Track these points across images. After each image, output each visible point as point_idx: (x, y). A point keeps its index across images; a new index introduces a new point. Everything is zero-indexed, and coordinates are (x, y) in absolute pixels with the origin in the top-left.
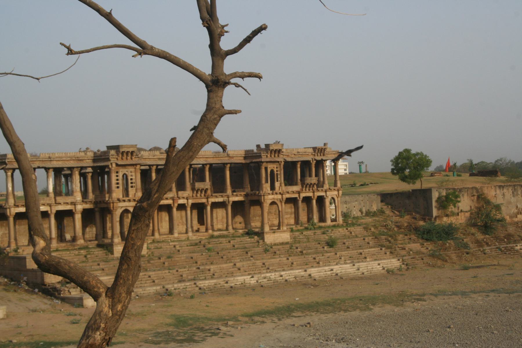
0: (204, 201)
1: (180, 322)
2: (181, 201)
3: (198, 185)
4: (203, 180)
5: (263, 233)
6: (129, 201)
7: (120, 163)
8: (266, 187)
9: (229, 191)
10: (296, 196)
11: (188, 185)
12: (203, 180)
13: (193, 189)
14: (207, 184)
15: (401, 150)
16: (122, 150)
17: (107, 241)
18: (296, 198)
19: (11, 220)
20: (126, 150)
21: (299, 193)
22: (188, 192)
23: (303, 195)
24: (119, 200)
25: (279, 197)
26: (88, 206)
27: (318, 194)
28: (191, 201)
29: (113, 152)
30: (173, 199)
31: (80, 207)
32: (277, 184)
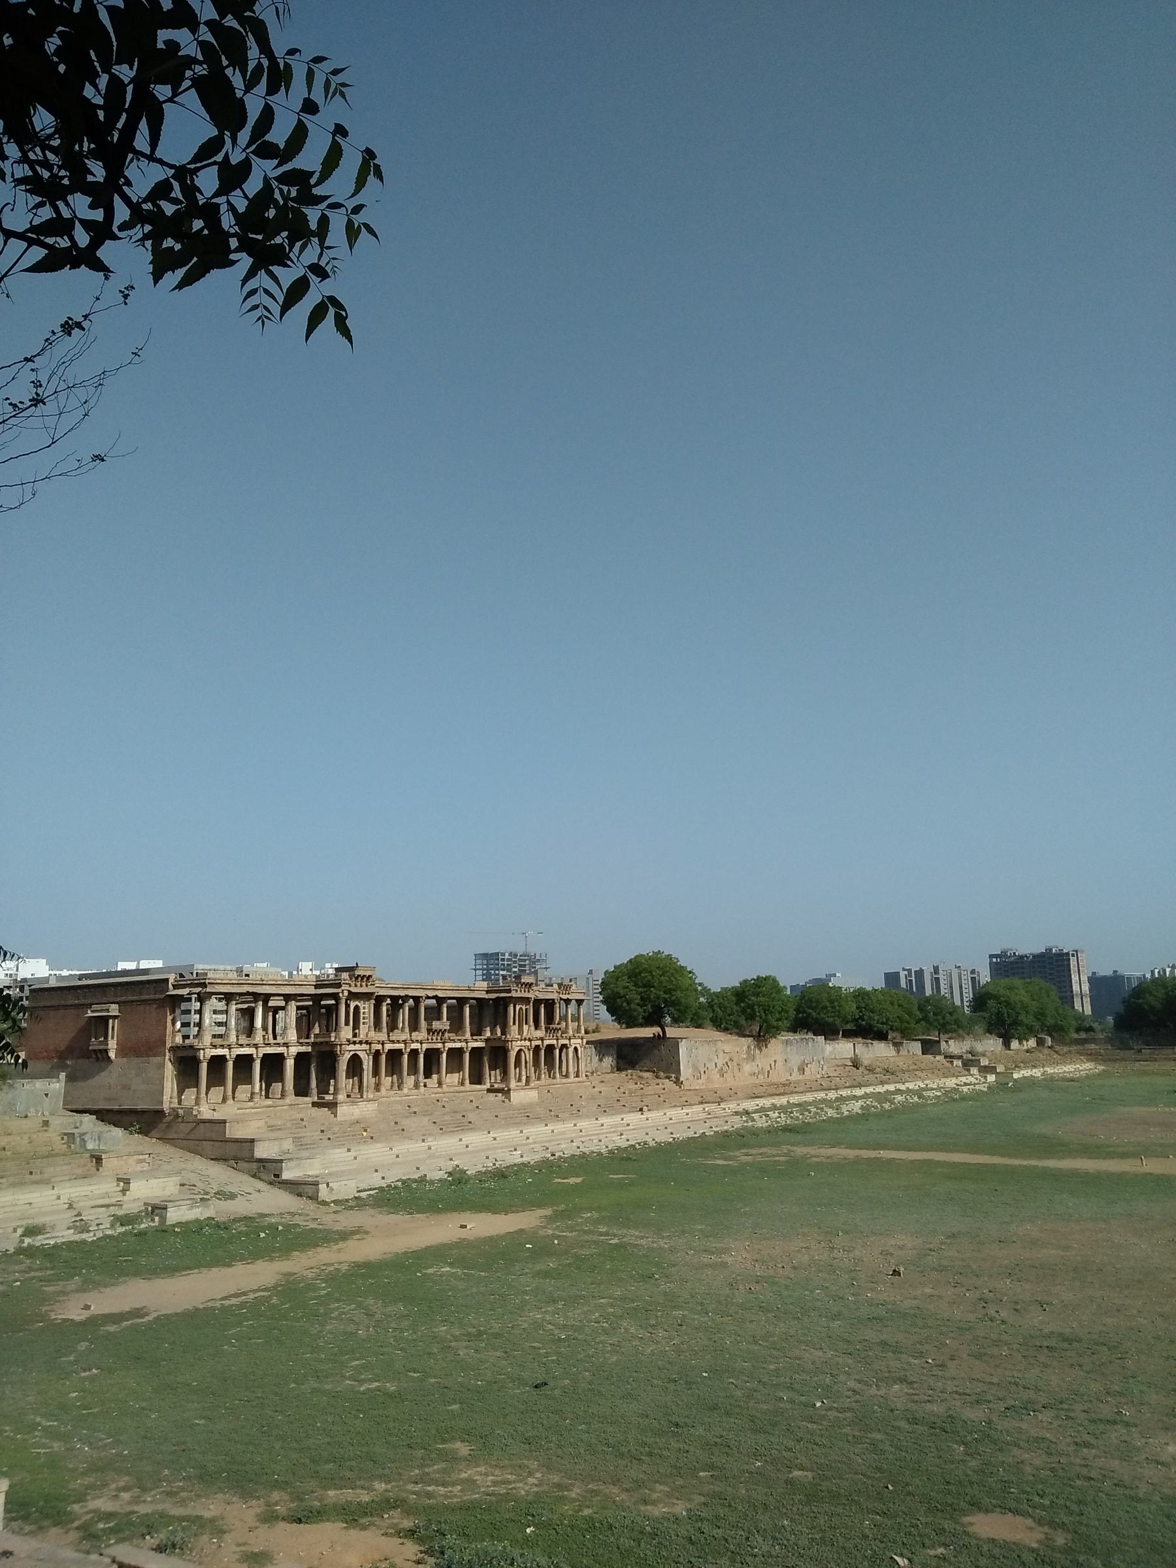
0: (440, 1046)
1: (569, 1218)
2: (415, 1046)
3: (436, 1025)
4: (439, 1018)
5: (509, 1090)
6: (361, 1043)
7: (354, 990)
8: (514, 1029)
9: (468, 1035)
10: (402, 1046)
11: (423, 1024)
12: (439, 1018)
13: (429, 1031)
14: (443, 1024)
15: (751, 975)
16: (357, 973)
17: (329, 1098)
18: (224, 1056)
19: (204, 1067)
20: (362, 973)
21: (542, 1039)
22: (422, 1035)
23: (547, 1042)
24: (348, 1040)
25: (528, 1043)
26: (303, 1049)
27: (562, 1042)
28: (425, 1046)
29: (345, 975)
30: (405, 1042)
31: (294, 1050)
32: (525, 1027)
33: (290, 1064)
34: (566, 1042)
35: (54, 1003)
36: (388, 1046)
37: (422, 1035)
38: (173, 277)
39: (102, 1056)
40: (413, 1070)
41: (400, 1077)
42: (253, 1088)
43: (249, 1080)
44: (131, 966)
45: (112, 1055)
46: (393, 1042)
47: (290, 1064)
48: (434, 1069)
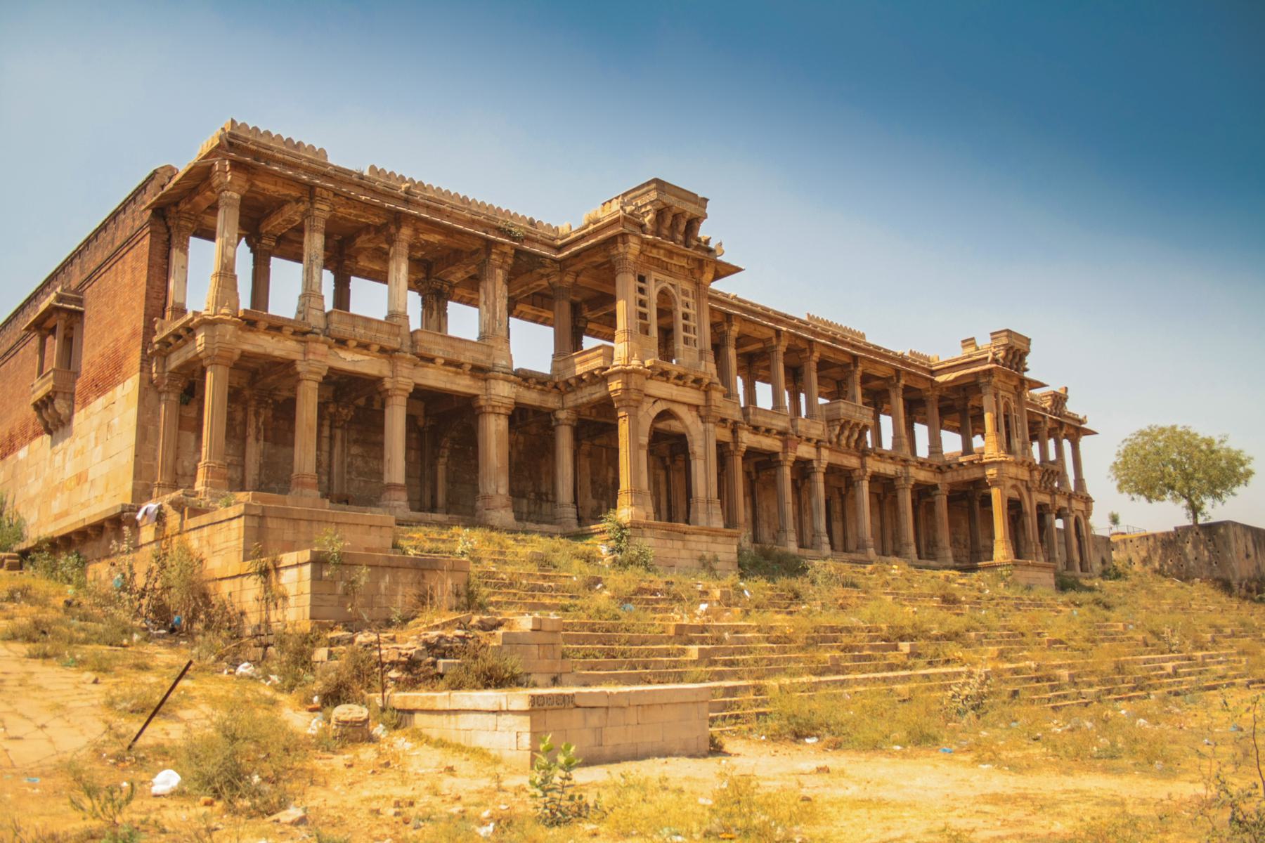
0: (853, 462)
2: (805, 451)
35: (99, 259)
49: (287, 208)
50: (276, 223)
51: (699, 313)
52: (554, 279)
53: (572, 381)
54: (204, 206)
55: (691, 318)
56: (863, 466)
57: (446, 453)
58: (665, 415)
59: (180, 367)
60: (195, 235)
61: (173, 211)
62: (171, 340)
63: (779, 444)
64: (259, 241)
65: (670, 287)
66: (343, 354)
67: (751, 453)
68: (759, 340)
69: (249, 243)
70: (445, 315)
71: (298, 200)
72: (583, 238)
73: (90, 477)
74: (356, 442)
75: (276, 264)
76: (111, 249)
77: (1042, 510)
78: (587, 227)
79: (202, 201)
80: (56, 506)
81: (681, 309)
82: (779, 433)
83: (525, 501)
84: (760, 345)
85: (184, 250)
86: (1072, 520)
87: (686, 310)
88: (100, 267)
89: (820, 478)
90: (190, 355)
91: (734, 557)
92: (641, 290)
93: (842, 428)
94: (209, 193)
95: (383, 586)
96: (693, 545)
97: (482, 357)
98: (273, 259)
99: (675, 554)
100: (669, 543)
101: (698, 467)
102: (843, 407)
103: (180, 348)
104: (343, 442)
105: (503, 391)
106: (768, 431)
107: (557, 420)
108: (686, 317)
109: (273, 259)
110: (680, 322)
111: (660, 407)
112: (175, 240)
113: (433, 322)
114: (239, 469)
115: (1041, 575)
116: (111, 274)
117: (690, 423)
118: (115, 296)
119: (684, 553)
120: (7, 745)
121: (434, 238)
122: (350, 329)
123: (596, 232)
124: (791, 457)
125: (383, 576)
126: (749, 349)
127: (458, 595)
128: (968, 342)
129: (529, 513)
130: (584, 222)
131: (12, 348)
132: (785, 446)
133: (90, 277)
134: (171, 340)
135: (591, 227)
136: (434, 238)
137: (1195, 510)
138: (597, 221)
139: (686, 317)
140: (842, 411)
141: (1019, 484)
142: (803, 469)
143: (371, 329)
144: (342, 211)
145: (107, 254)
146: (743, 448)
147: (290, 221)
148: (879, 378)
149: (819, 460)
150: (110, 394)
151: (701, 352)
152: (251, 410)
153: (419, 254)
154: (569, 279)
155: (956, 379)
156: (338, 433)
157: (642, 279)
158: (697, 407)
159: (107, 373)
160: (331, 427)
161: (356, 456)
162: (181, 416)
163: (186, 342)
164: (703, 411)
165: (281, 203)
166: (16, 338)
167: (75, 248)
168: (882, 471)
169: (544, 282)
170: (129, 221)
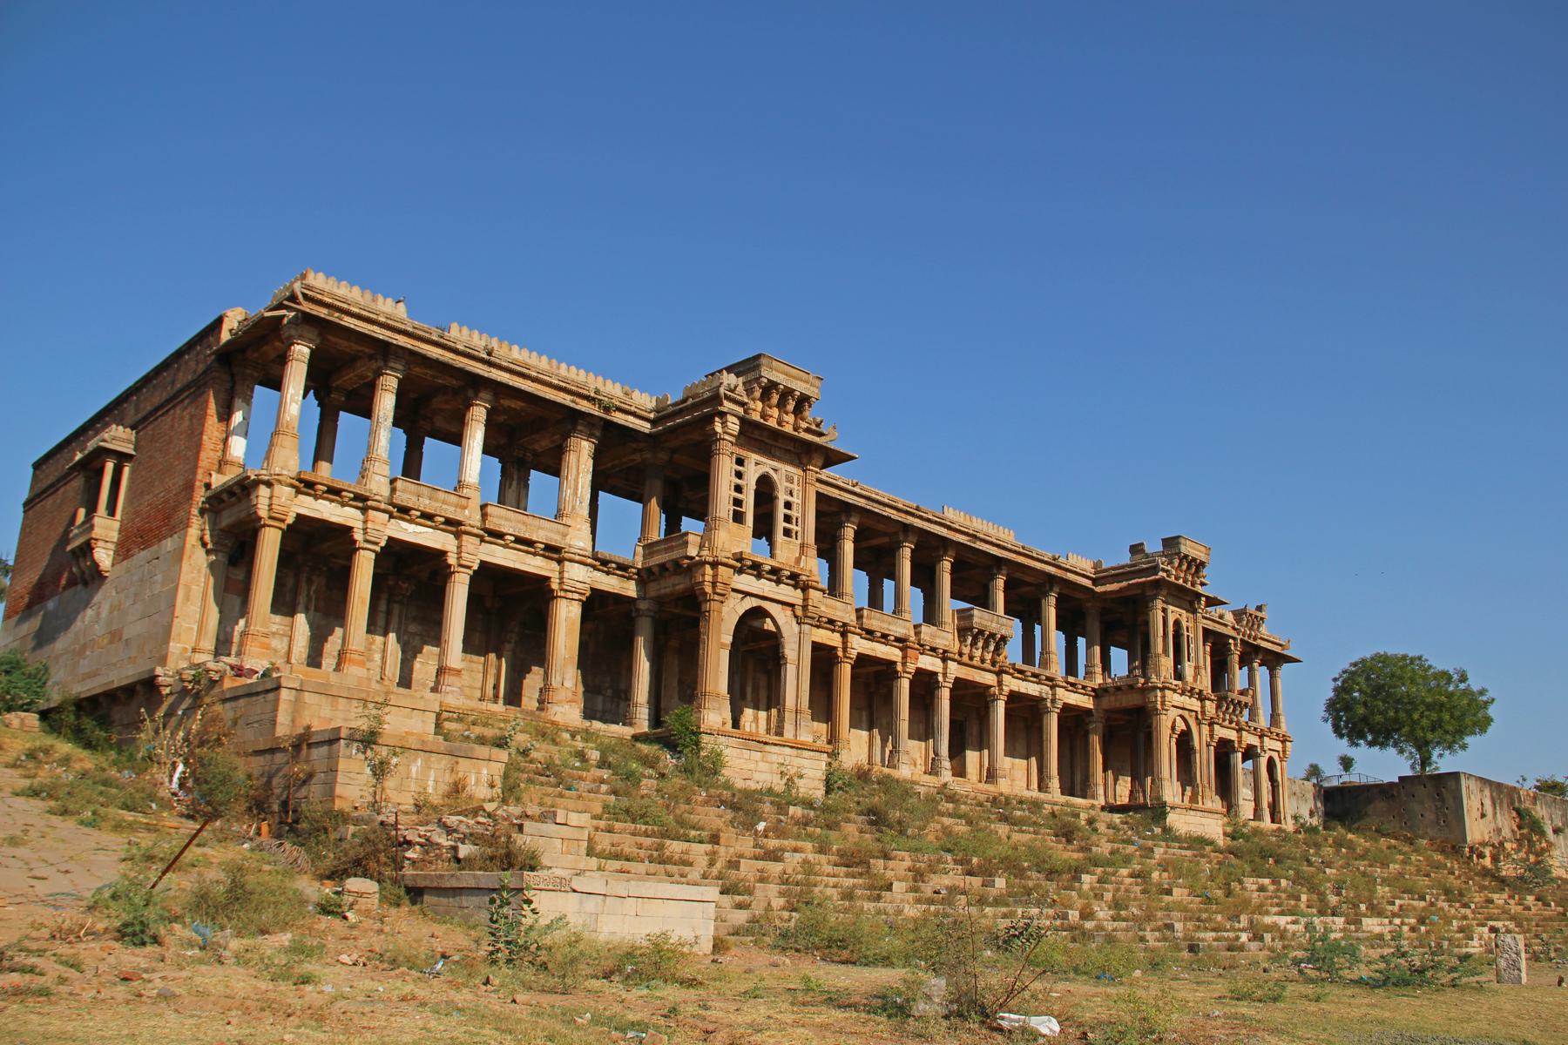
0: (989, 679)
2: (929, 663)
10: (893, 653)
30: (901, 641)
33: (566, 619)
34: (1254, 741)
35: (157, 399)
36: (859, 645)
37: (945, 637)
38: (16, 618)
39: (95, 577)
40: (924, 728)
41: (889, 731)
42: (442, 654)
43: (983, 742)
44: (478, 341)
45: (104, 556)
46: (870, 634)
47: (566, 619)
48: (973, 730)
49: (359, 363)
50: (348, 379)
51: (804, 503)
52: (647, 455)
53: (656, 570)
54: (273, 355)
55: (794, 507)
56: (1000, 683)
57: (514, 637)
58: (758, 613)
59: (232, 526)
60: (262, 384)
61: (236, 365)
62: (225, 496)
63: (898, 653)
64: (328, 394)
65: (772, 473)
66: (404, 525)
67: (863, 661)
68: (885, 534)
69: (317, 396)
70: (527, 486)
71: (371, 357)
72: (680, 413)
73: (125, 637)
74: (414, 619)
75: (344, 417)
76: (170, 391)
77: (1224, 750)
78: (685, 401)
79: (270, 351)
80: (84, 666)
81: (782, 497)
82: (898, 640)
83: (600, 698)
84: (886, 540)
85: (248, 400)
86: (1263, 761)
87: (789, 498)
88: (156, 410)
89: (945, 695)
90: (243, 515)
91: (821, 775)
92: (739, 475)
93: (975, 639)
94: (278, 344)
95: (414, 770)
96: (774, 758)
97: (558, 538)
98: (342, 413)
99: (752, 766)
100: (746, 753)
101: (790, 671)
102: (980, 617)
103: (233, 505)
104: (400, 617)
105: (580, 576)
106: (884, 636)
107: (638, 610)
108: (788, 505)
109: (342, 413)
110: (781, 511)
111: (750, 603)
112: (239, 388)
113: (511, 494)
114: (286, 640)
115: (1204, 821)
116: (168, 419)
117: (783, 619)
118: (171, 442)
119: (763, 766)
120: (33, 882)
121: (516, 404)
122: (414, 499)
123: (695, 407)
124: (911, 668)
125: (415, 760)
126: (875, 542)
127: (492, 786)
128: (1136, 549)
129: (604, 712)
130: (679, 397)
131: (52, 485)
132: (904, 657)
133: (145, 419)
134: (225, 496)
135: (690, 401)
136: (516, 404)
137: (1425, 761)
138: (697, 395)
139: (788, 505)
140: (976, 620)
141: (1186, 714)
142: (925, 684)
143: (437, 500)
144: (417, 370)
145: (165, 396)
146: (853, 654)
147: (361, 377)
148: (1029, 584)
149: (945, 675)
150: (155, 547)
151: (802, 546)
152: (304, 577)
153: (502, 418)
154: (663, 456)
155: (1121, 589)
156: (396, 608)
157: (740, 462)
158: (792, 606)
159: (154, 525)
160: (389, 602)
161: (415, 634)
162: (227, 578)
163: (240, 500)
164: (803, 615)
165: (353, 359)
166: (57, 474)
167: (131, 383)
168: (1023, 690)
169: (637, 457)
170: (192, 364)
